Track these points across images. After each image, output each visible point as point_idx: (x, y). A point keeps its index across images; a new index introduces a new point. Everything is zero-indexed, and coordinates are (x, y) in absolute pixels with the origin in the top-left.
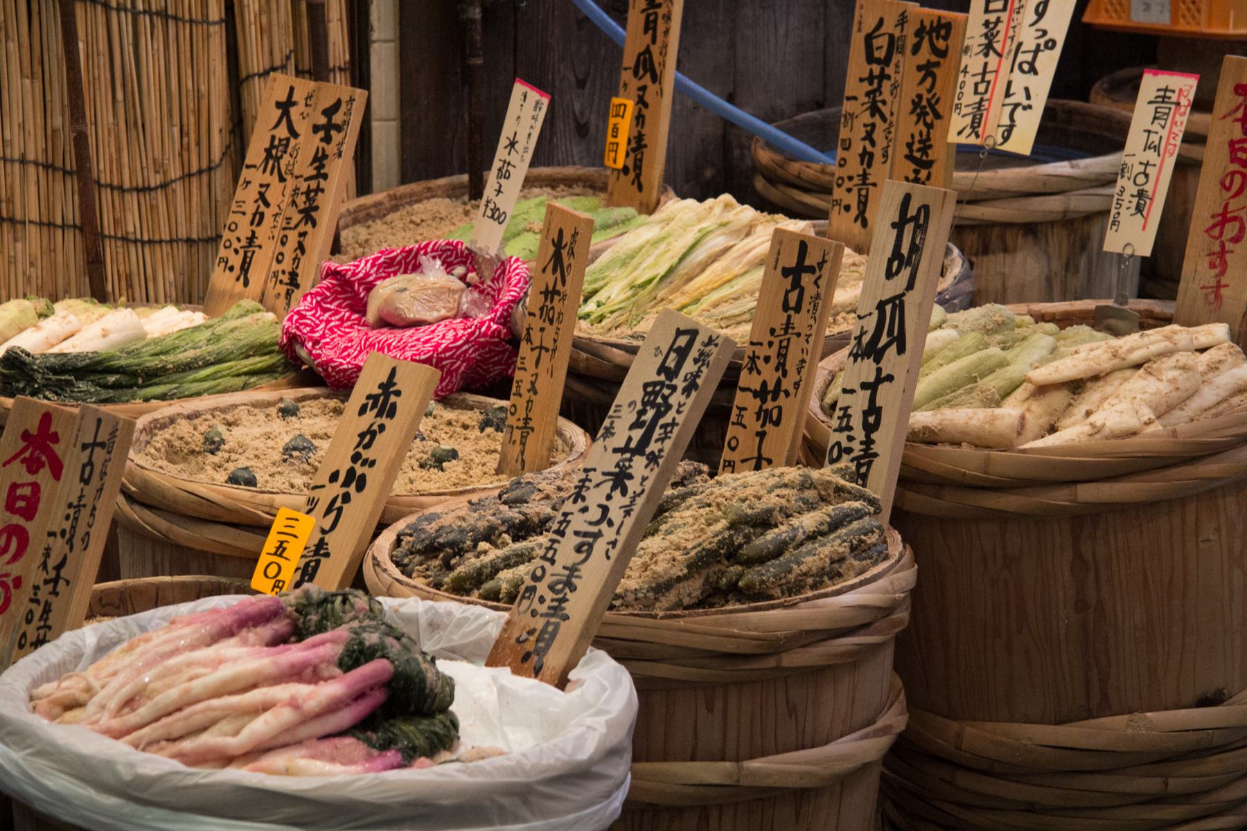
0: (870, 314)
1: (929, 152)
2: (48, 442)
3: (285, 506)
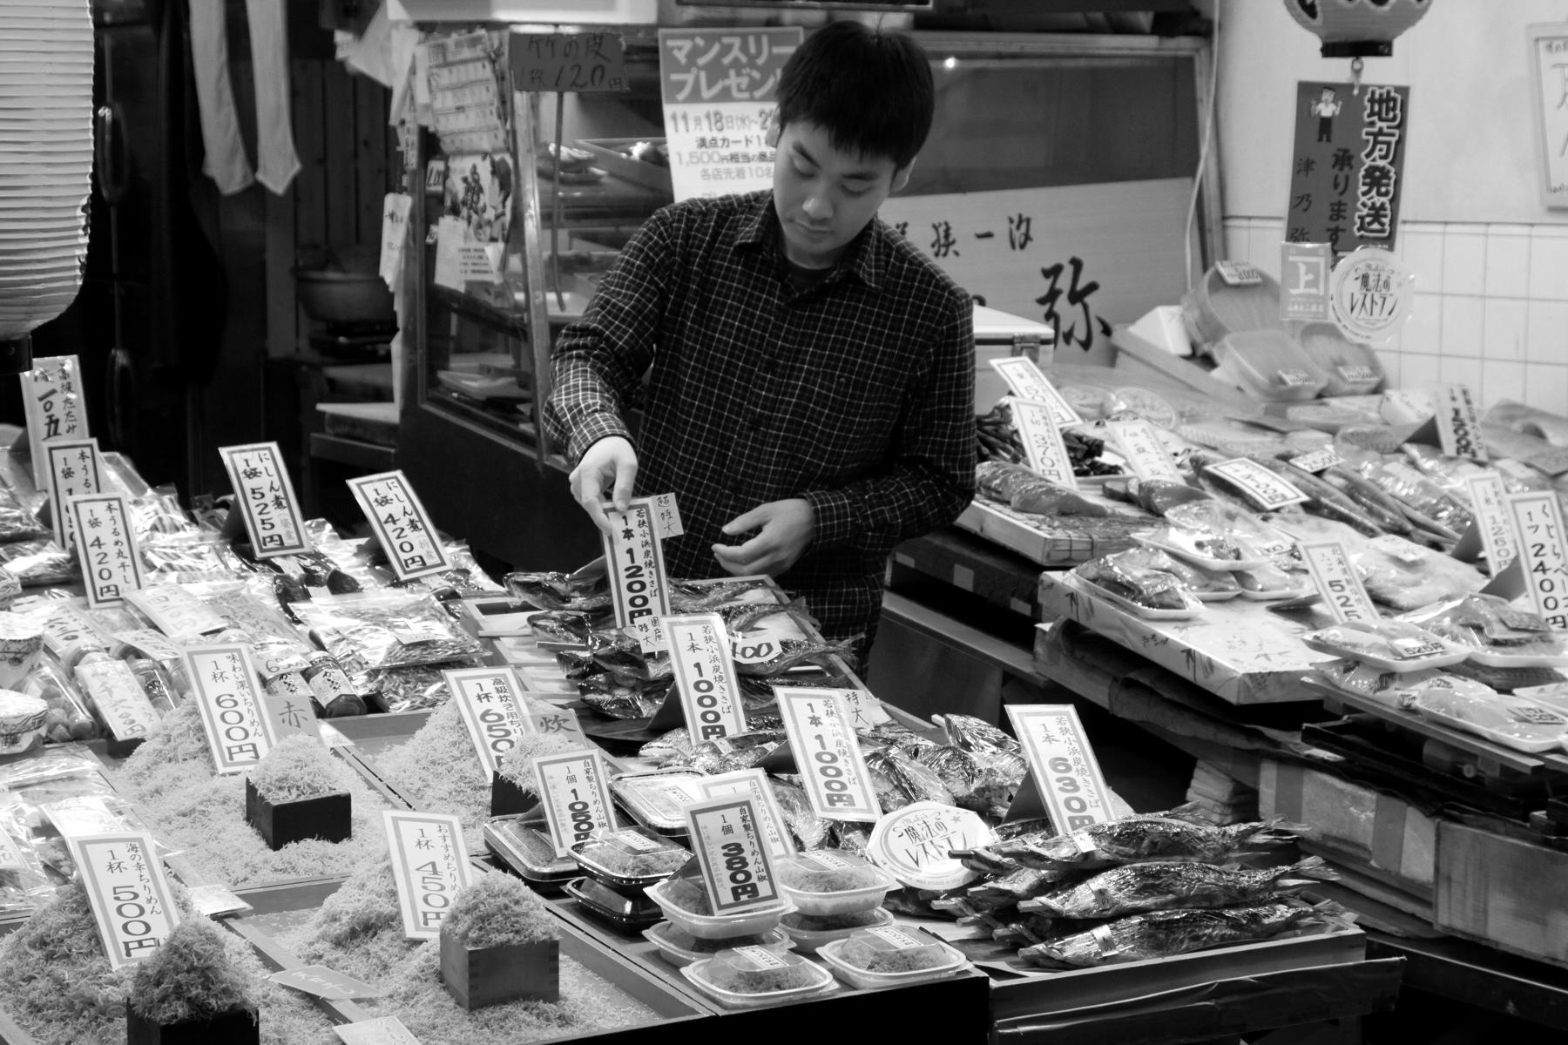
0: (810, 705)
2: (1339, 757)
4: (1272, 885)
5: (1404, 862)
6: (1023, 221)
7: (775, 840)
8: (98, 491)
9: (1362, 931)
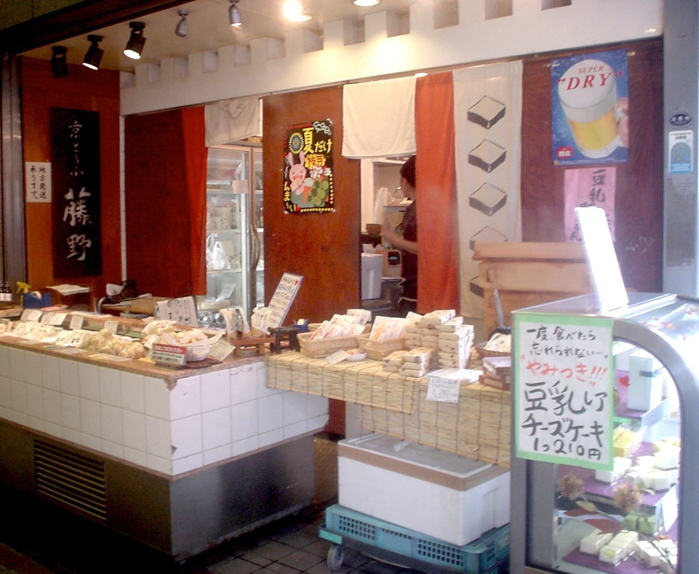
1: (41, 175)
4: (229, 364)
5: (44, 58)
7: (173, 350)
8: (599, 458)
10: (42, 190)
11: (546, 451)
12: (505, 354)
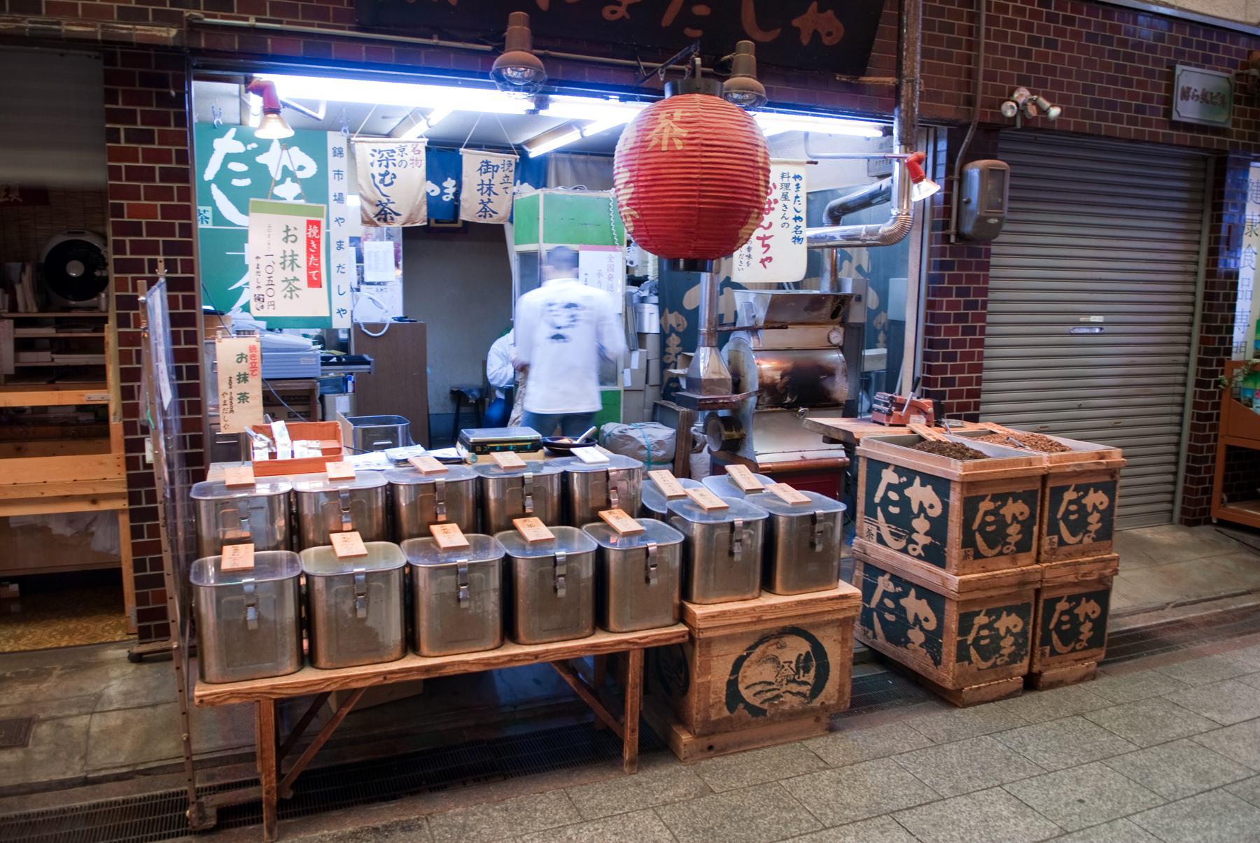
3: (475, 145)
6: (337, 220)
7: (631, 543)
9: (866, 649)
10: (610, 282)
11: (334, 149)
12: (1037, 582)
